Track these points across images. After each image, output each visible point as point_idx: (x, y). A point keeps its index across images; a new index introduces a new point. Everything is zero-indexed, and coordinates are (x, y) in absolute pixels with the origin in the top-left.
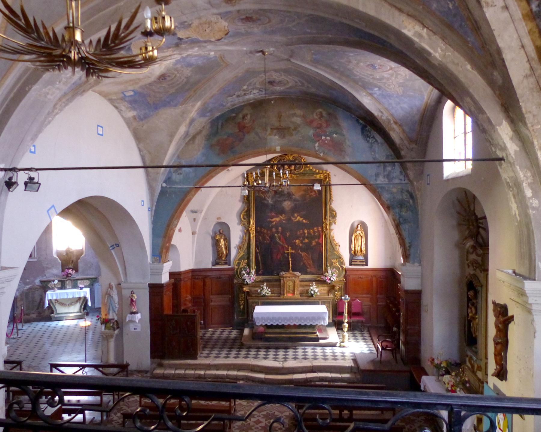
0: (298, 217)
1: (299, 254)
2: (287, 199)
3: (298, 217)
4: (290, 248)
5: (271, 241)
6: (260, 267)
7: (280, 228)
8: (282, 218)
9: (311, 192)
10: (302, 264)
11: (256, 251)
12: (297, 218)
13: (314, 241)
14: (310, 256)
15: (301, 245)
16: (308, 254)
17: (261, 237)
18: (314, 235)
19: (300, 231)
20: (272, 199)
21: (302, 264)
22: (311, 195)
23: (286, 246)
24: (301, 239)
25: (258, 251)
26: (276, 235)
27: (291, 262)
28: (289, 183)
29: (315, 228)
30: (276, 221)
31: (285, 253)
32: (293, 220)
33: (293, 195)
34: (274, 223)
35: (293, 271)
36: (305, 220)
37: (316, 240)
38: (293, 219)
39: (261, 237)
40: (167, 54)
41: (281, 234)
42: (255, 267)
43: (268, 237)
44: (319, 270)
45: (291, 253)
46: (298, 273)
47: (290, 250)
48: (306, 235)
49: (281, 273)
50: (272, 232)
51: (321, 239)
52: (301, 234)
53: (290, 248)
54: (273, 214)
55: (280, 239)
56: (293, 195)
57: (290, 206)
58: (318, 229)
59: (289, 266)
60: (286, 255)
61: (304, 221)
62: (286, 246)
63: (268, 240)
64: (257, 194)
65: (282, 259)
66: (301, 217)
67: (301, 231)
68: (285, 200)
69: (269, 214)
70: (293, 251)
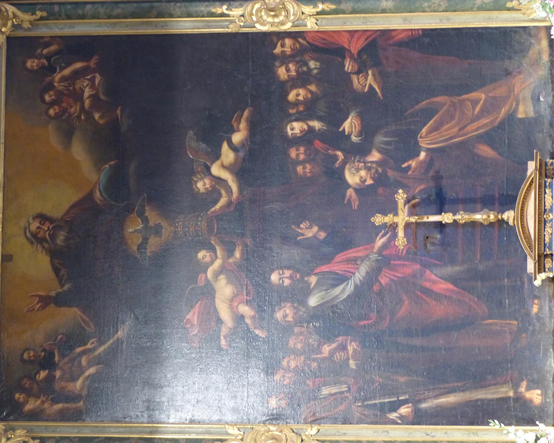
0: (216, 170)
9: (78, 97)
10: (485, 151)
11: (404, 420)
12: (219, 180)
15: (375, 156)
17: (325, 391)
21: (485, 151)
25: (404, 410)
26: (313, 301)
29: (282, 72)
30: (232, 300)
37: (349, 66)
38: (223, 201)
48: (316, 125)
55: (341, 279)
58: (285, 59)
61: (237, 138)
63: (343, 348)
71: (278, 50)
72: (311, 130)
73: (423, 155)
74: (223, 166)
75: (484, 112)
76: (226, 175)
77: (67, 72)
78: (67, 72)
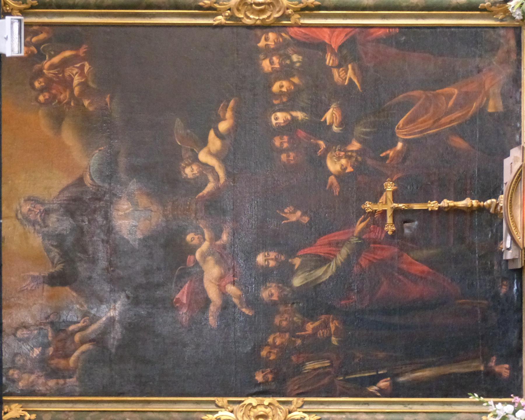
1: (404, 156)
2: (100, 219)
3: (203, 156)
4: (368, 206)
5: (330, 310)
6: (476, 374)
7: (260, 259)
8: (205, 246)
9: (68, 84)
10: (459, 143)
11: (383, 393)
12: (205, 166)
13: (336, 74)
14: (416, 93)
15: (355, 146)
16: (404, 107)
17: (310, 366)
18: (302, 72)
19: (281, 151)
20: (101, 301)
21: (459, 143)
22: (84, 85)
23: (360, 226)
24: (322, 144)
25: (383, 384)
26: (297, 282)
27: (446, 203)
28: (116, 358)
29: (266, 65)
30: (221, 278)
31: (398, 234)
32: (218, 189)
33: (80, 181)
34: (231, 289)
35: (496, 192)
36: (220, 119)
37: (330, 60)
38: (210, 187)
39: (310, 366)
40: (337, 120)
41: (292, 253)
42: (475, 398)
43: (310, 327)
44: (494, 48)
45: (395, 201)
46: (507, 162)
47: (379, 207)
48: (299, 115)
49: (509, 255)
50: (284, 301)
51: (325, 36)
52: (295, 144)
53: (368, 206)
54: (183, 296)
55: (324, 261)
56: (80, 181)
57: (144, 201)
58: (268, 52)
59: (470, 211)
60: (409, 229)
61: (223, 126)
62: (360, 226)
63: (325, 325)
64: (71, 381)
65: (425, 253)
66: (204, 142)
67: (277, 142)
68: (109, 230)
69: (184, 314)
70: (390, 187)
71: (262, 44)
72: (294, 119)
73: (400, 145)
74: (210, 153)
75: (458, 106)
76: (212, 162)
77: (56, 60)
78: (56, 60)
